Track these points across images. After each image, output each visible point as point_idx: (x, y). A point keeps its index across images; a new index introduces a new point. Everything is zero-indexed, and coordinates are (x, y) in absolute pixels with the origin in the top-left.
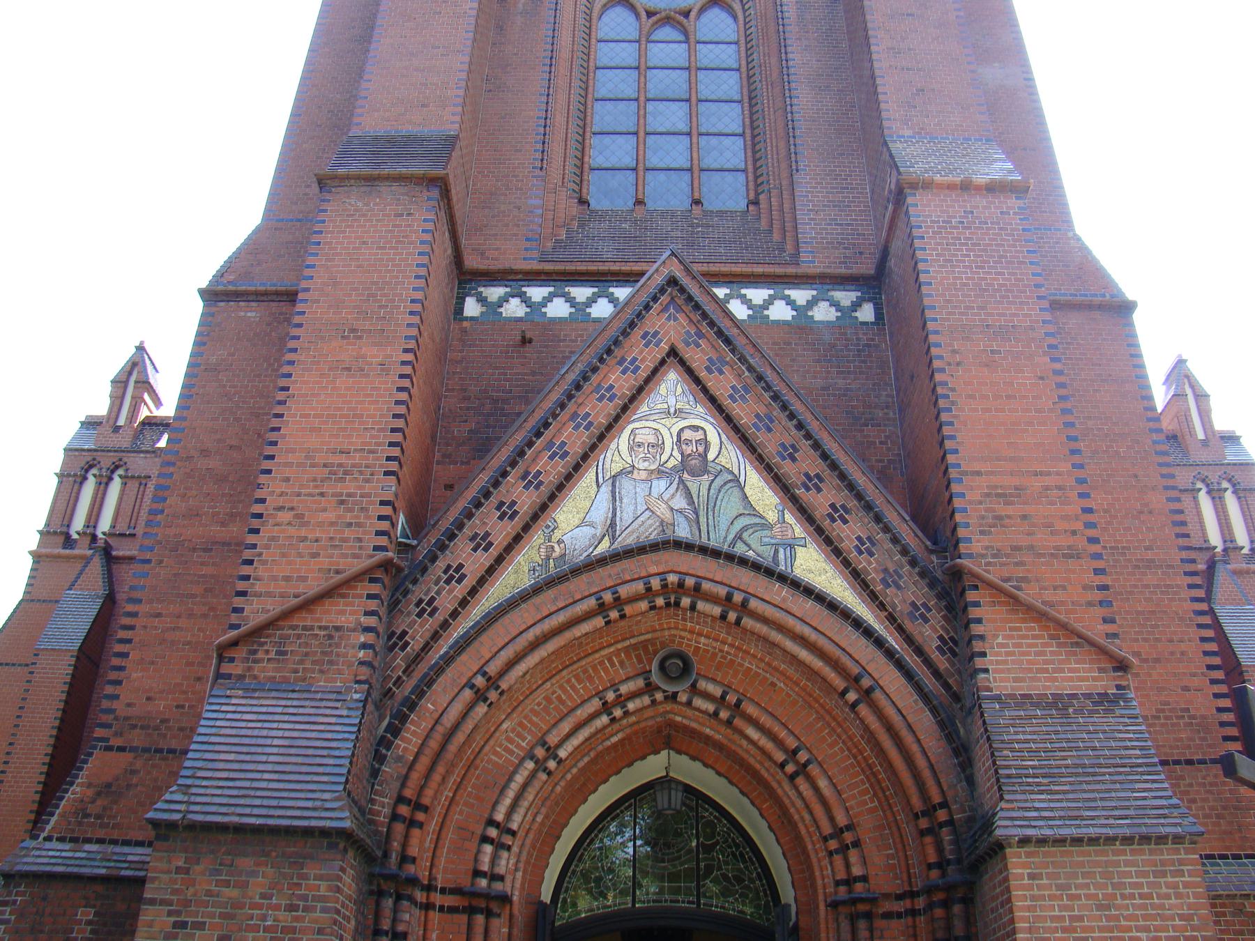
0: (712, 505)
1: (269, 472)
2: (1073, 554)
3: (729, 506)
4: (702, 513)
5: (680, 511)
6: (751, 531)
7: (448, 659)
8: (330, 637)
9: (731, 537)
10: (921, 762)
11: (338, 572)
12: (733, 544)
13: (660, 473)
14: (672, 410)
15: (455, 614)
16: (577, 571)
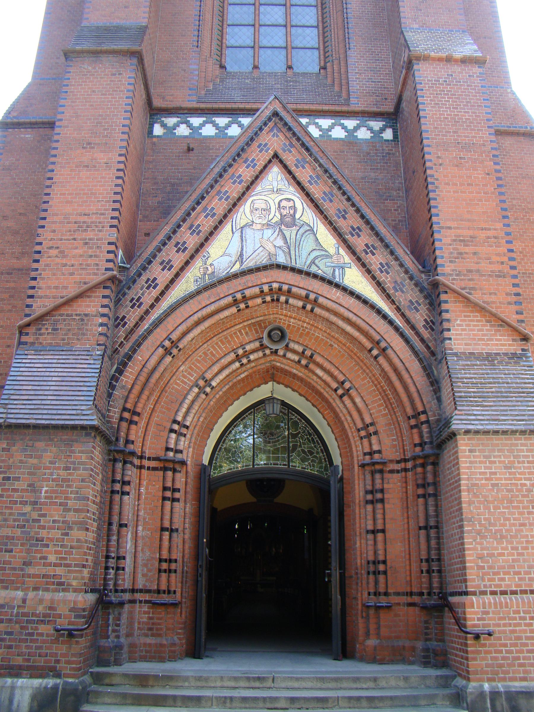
0: (298, 245)
1: (43, 227)
2: (501, 275)
3: (308, 244)
4: (292, 249)
5: (280, 248)
6: (320, 259)
7: (149, 332)
8: (82, 320)
9: (308, 262)
10: (412, 389)
11: (85, 283)
12: (310, 266)
13: (268, 225)
14: (275, 190)
15: (152, 306)
16: (221, 281)
